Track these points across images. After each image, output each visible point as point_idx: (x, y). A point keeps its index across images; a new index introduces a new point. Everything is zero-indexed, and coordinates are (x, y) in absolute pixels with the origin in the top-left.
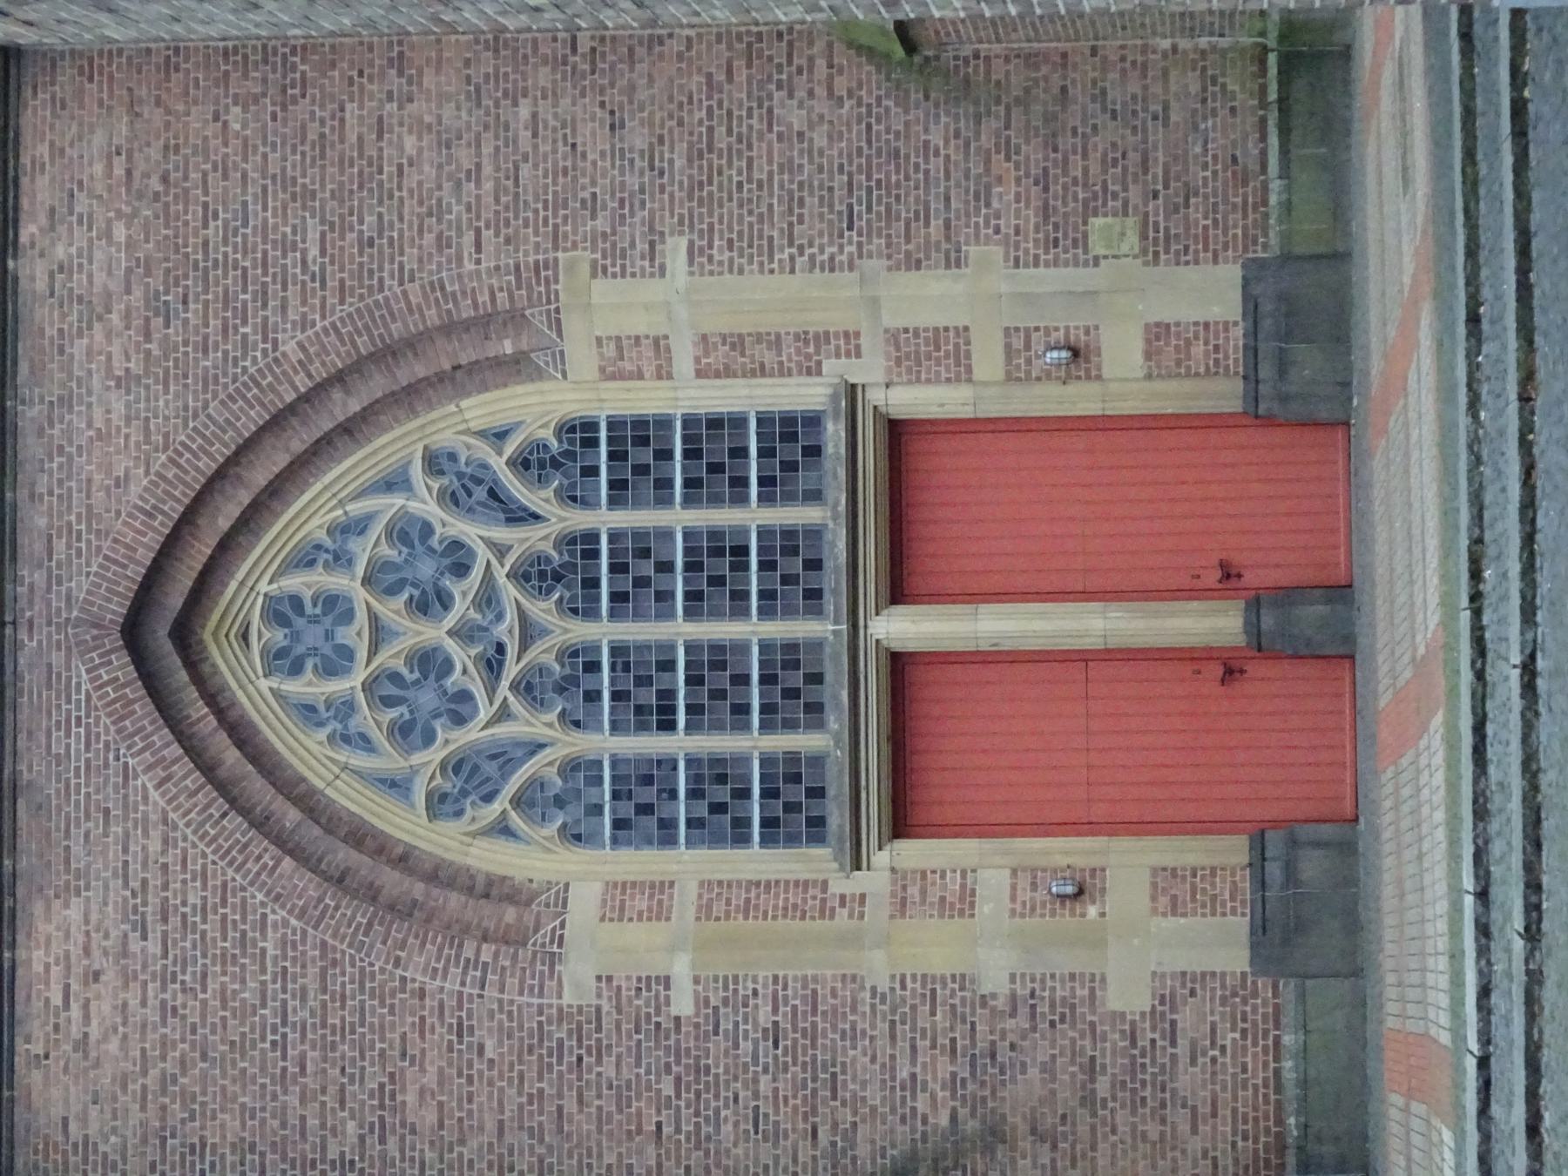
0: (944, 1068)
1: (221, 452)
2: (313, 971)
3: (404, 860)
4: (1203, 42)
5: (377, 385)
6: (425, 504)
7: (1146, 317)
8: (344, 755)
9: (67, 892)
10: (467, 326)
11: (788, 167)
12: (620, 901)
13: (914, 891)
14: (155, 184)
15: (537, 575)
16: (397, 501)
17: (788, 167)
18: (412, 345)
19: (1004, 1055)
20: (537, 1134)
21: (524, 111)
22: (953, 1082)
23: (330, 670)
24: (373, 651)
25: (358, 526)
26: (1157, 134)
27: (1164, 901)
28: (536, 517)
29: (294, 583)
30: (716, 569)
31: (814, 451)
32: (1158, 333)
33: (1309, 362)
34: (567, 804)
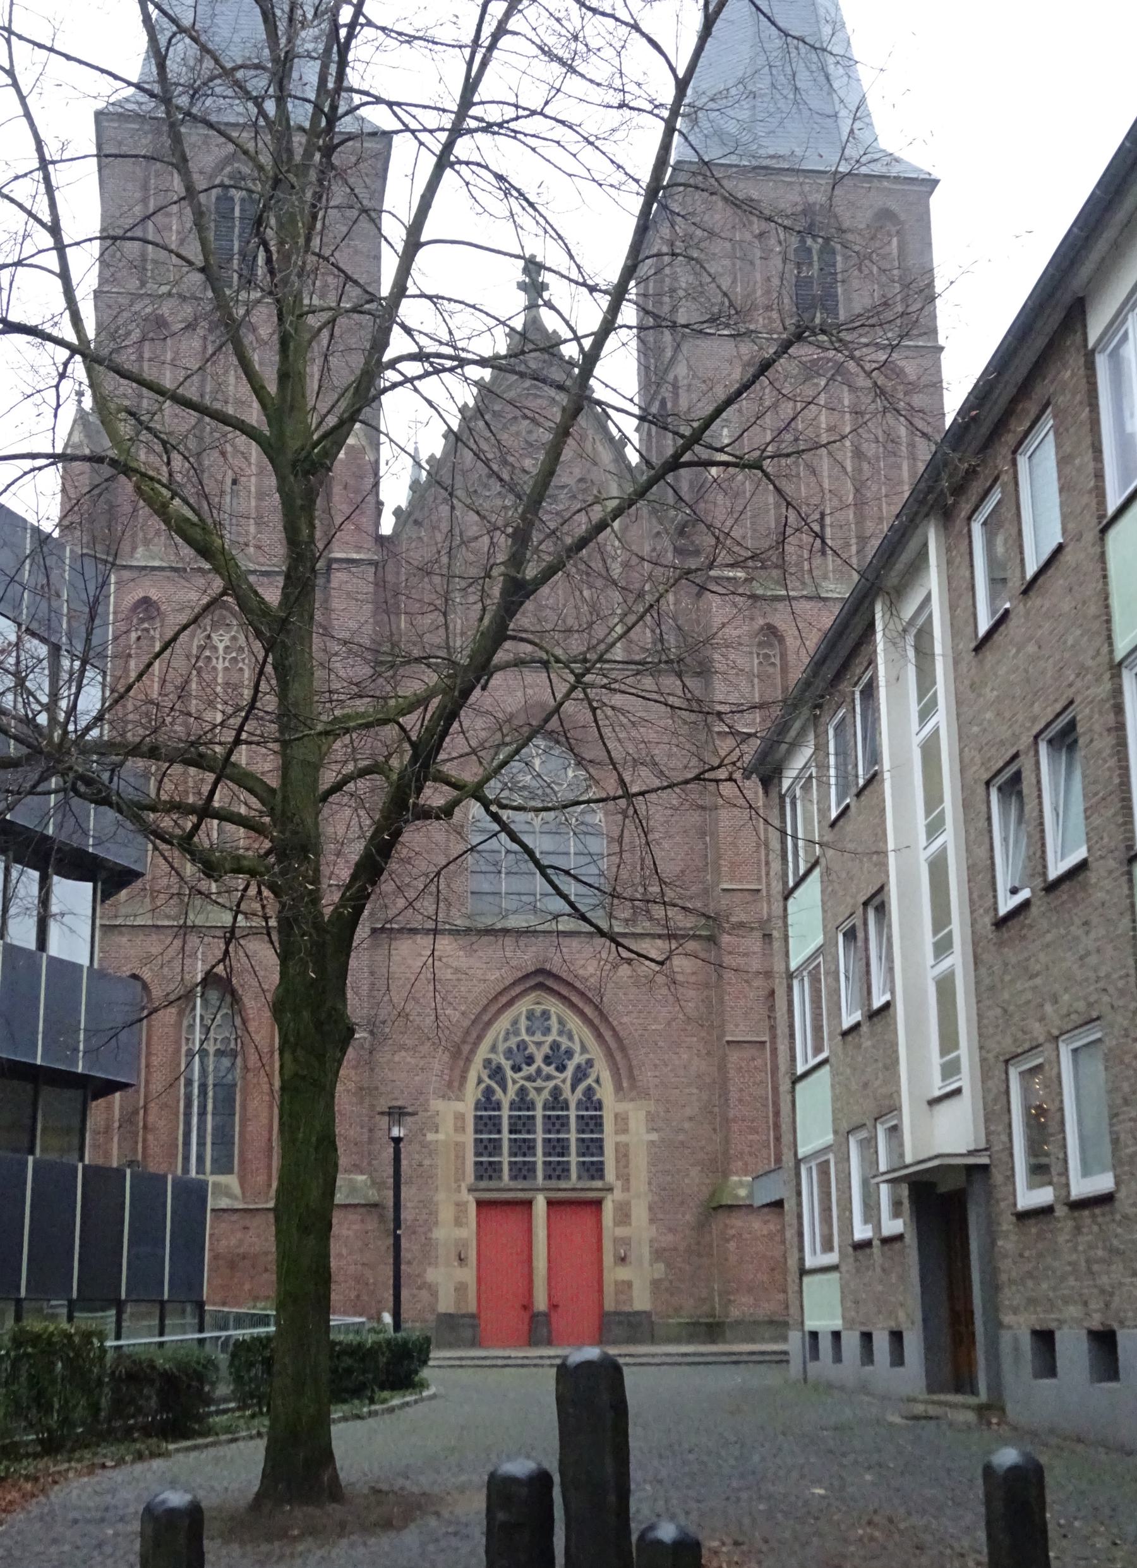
3: (473, 1051)
5: (613, 1044)
6: (578, 1059)
12: (459, 1117)
15: (556, 1092)
18: (626, 1056)
23: (528, 1030)
25: (571, 1038)
29: (554, 1019)
30: (558, 1147)
32: (629, 1284)
34: (488, 1101)
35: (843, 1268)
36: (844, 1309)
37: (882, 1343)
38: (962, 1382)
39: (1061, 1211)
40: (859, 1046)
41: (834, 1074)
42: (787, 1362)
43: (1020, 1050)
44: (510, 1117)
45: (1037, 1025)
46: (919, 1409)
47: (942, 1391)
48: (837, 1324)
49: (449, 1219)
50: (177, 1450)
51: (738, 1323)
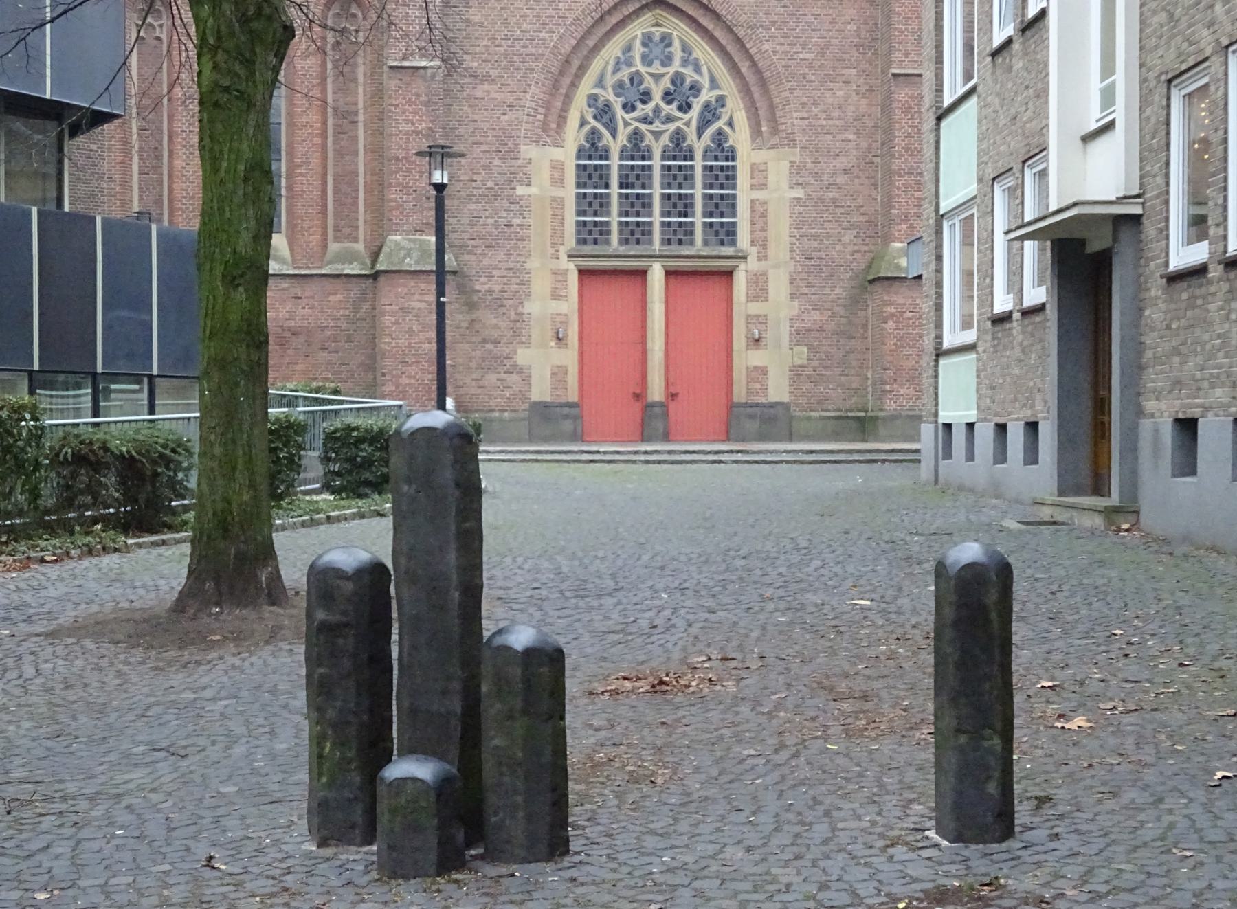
0: (497, 288)
2: (533, 51)
3: (574, 85)
4: (870, 389)
5: (751, 78)
6: (706, 95)
7: (770, 365)
8: (612, 63)
10: (773, 114)
12: (557, 167)
13: (560, 278)
15: (678, 137)
19: (501, 310)
20: (473, 134)
21: (851, 137)
22: (490, 291)
25: (697, 69)
26: (838, 371)
27: (556, 370)
28: (699, 138)
29: (677, 44)
31: (722, 243)
32: (763, 371)
33: (751, 426)
34: (593, 149)
35: (980, 349)
36: (980, 397)
37: (1016, 434)
38: (1099, 486)
39: (1215, 272)
40: (1010, 69)
41: (983, 106)
42: (919, 461)
43: (1184, 67)
44: (621, 167)
45: (1205, 32)
46: (1046, 513)
47: (1078, 491)
48: (972, 415)
49: (548, 293)
50: (139, 546)
51: (893, 418)
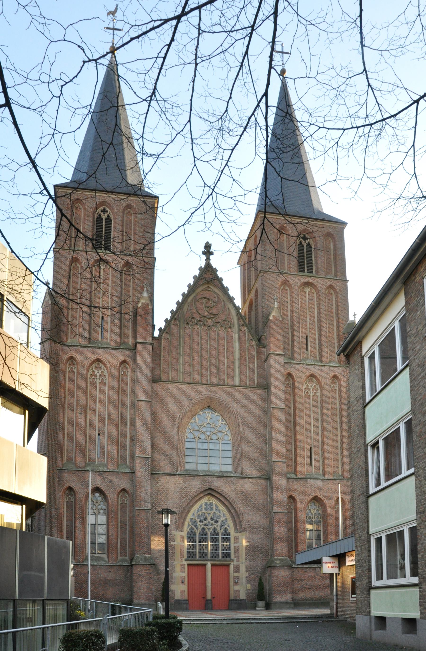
1: (228, 498)
6: (222, 518)
8: (197, 510)
9: (184, 481)
11: (256, 555)
14: (255, 493)
15: (215, 529)
16: (222, 516)
17: (256, 555)
18: (239, 518)
20: (159, 528)
21: (262, 529)
24: (207, 513)
25: (219, 511)
29: (214, 505)
32: (238, 591)
